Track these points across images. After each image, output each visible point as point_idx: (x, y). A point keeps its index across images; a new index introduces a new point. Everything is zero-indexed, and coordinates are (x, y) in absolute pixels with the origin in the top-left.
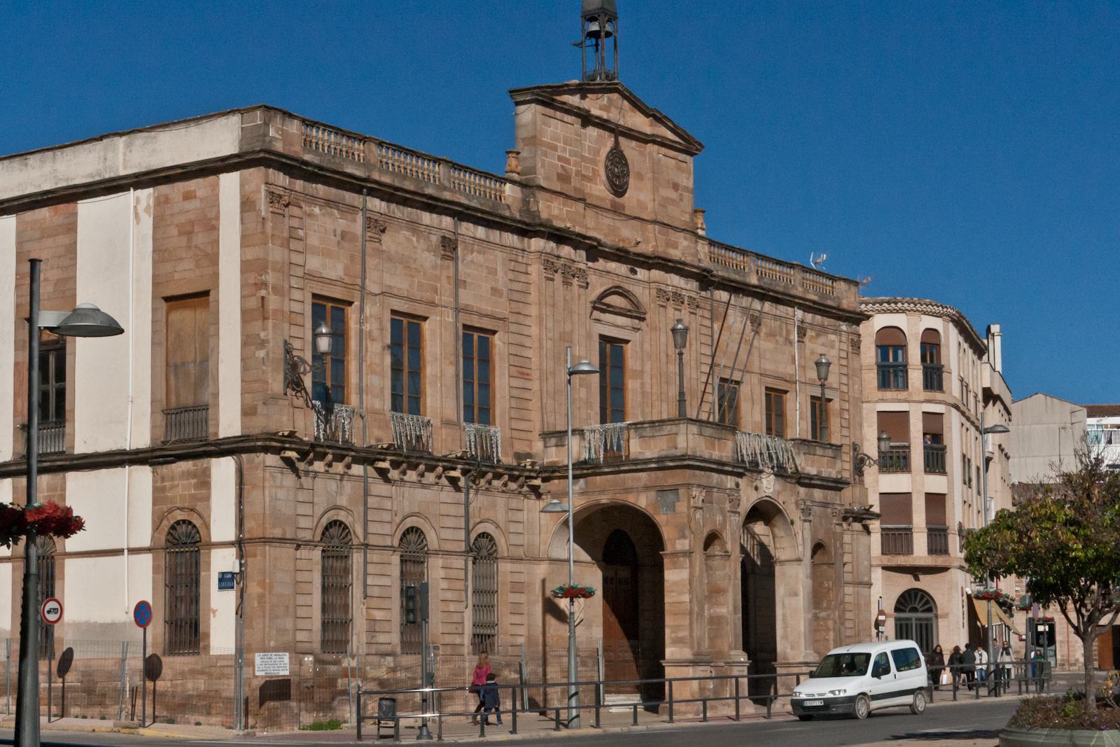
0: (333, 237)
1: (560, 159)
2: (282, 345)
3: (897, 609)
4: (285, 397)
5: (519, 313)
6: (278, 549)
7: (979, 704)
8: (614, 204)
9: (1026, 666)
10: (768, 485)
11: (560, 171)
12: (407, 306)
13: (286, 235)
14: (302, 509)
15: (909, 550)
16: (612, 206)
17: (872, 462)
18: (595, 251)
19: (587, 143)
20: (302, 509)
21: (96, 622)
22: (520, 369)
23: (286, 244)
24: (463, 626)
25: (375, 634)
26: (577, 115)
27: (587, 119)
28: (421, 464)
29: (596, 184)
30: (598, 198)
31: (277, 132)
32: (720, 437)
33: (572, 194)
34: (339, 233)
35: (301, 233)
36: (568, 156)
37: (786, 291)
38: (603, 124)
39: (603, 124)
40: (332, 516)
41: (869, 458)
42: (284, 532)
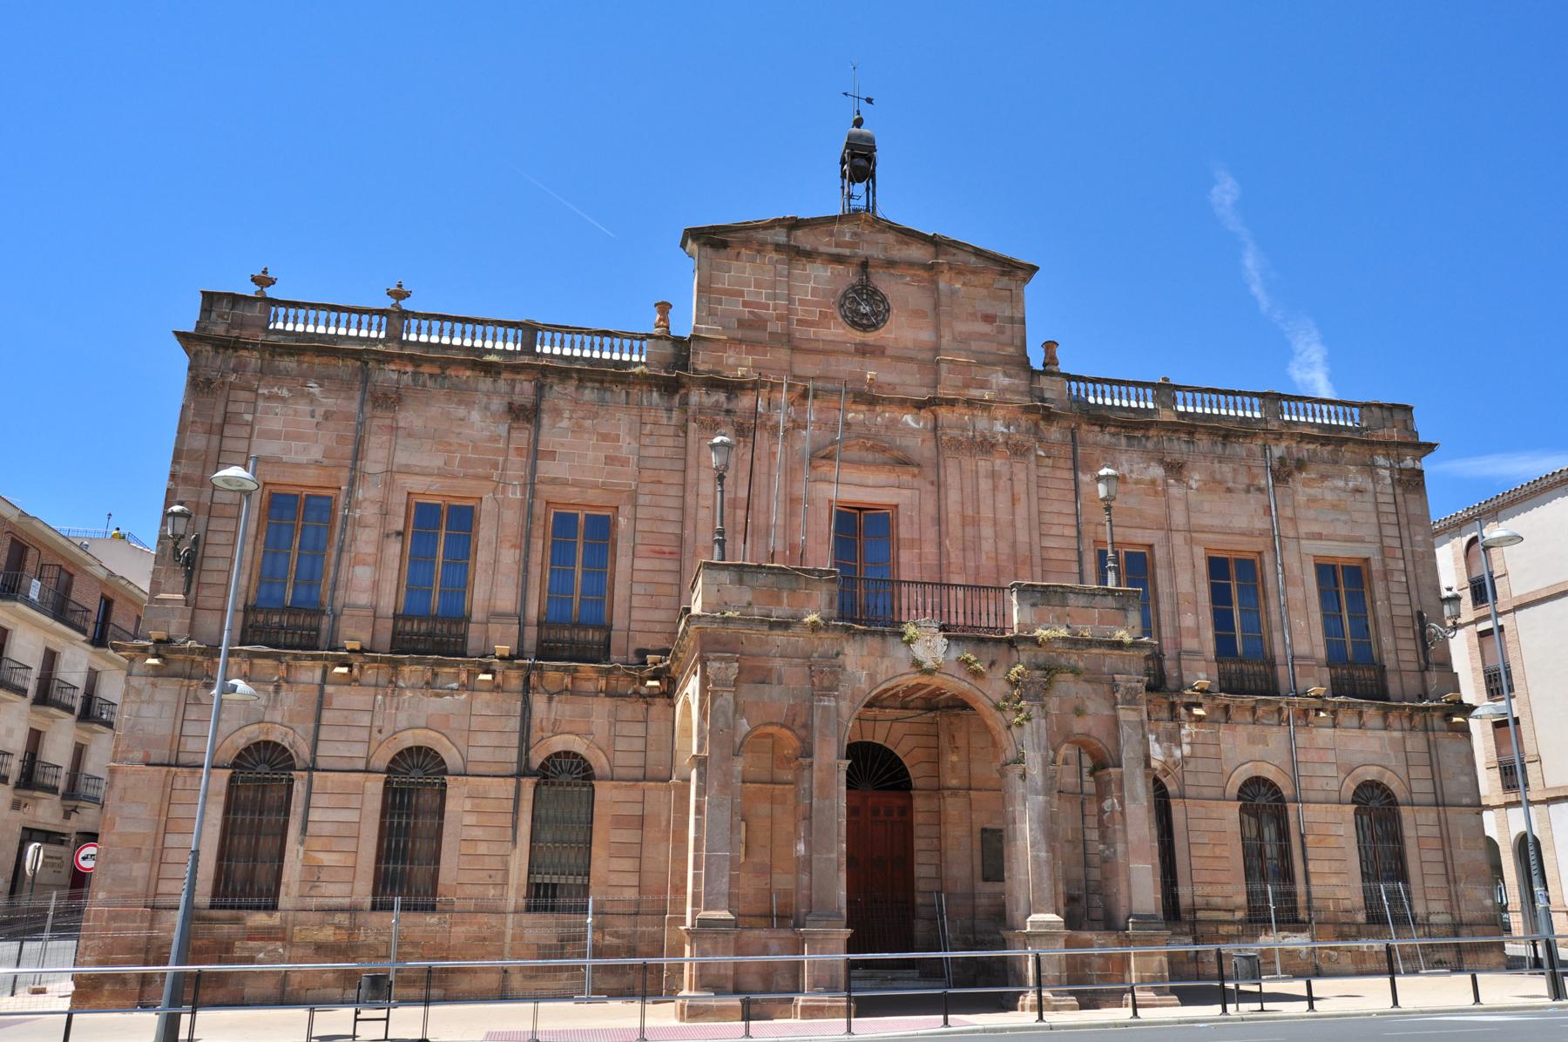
1: (745, 304)
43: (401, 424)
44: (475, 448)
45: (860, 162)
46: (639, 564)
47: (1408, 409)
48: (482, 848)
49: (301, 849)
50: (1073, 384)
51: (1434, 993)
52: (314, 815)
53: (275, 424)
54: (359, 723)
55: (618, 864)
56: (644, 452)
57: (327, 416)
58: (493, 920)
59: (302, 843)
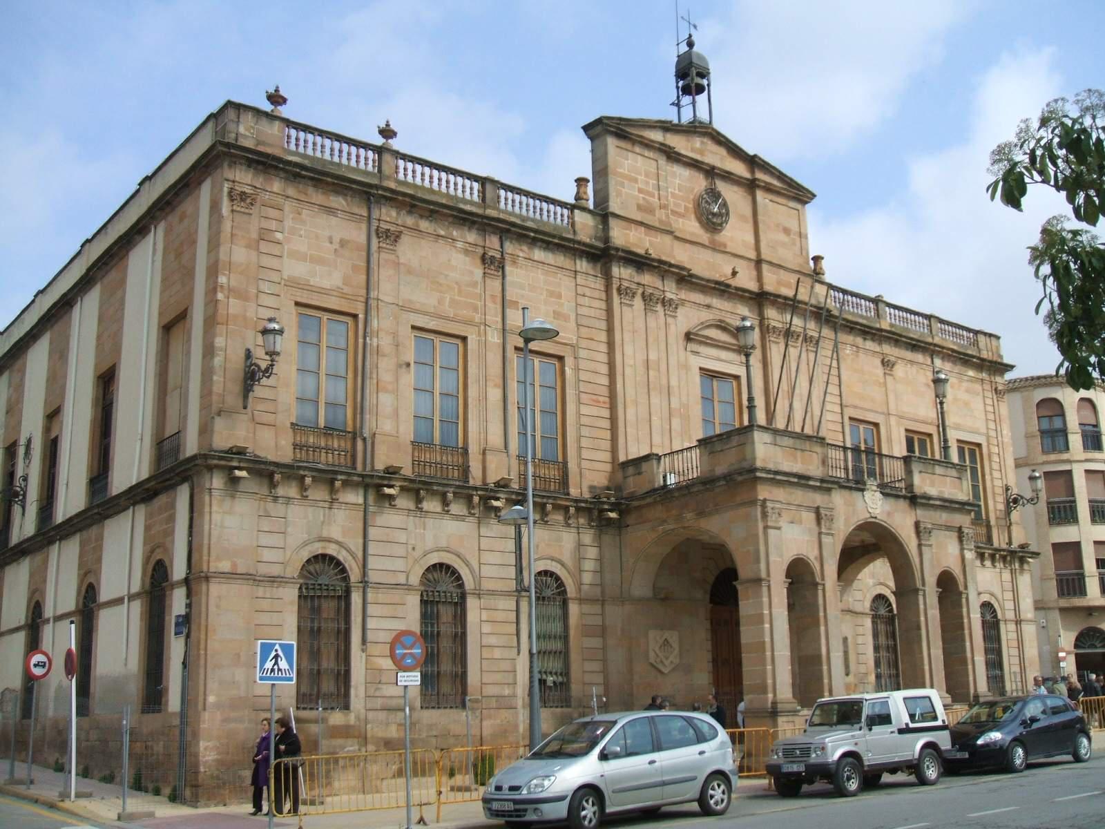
0: (328, 245)
1: (640, 191)
2: (242, 355)
3: (1076, 646)
4: (244, 411)
5: (592, 339)
6: (225, 586)
7: (284, 655)
8: (713, 241)
9: (447, 476)
10: (873, 505)
11: (641, 202)
12: (434, 323)
13: (254, 235)
14: (265, 540)
15: (1082, 591)
16: (710, 242)
17: (1025, 502)
18: (685, 279)
19: (677, 181)
20: (265, 540)
21: (1099, 749)
22: (594, 397)
23: (254, 245)
24: (515, 675)
25: (380, 686)
26: (660, 150)
27: (672, 156)
28: (448, 492)
29: (690, 220)
30: (692, 234)
31: (246, 129)
32: (803, 448)
33: (657, 224)
34: (336, 239)
35: (279, 236)
36: (651, 190)
37: (921, 339)
38: (695, 165)
39: (695, 165)
40: (318, 548)
41: (1022, 498)
42: (234, 565)
43: (402, 261)
44: (460, 292)
45: (691, 76)
46: (585, 410)
47: (998, 338)
48: (497, 653)
49: (364, 655)
50: (401, 163)
51: (165, 811)
52: (371, 624)
53: (300, 245)
54: (407, 541)
55: (590, 666)
56: (582, 311)
57: (343, 243)
58: (505, 714)
59: (363, 651)
